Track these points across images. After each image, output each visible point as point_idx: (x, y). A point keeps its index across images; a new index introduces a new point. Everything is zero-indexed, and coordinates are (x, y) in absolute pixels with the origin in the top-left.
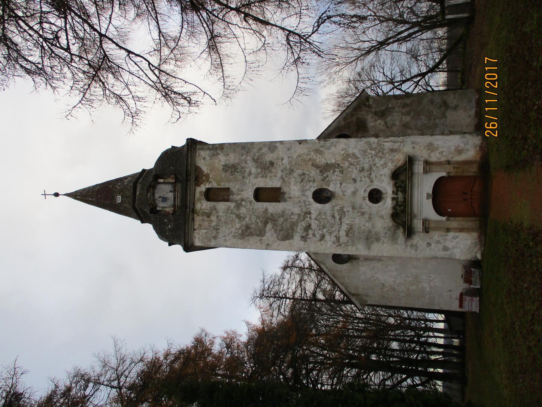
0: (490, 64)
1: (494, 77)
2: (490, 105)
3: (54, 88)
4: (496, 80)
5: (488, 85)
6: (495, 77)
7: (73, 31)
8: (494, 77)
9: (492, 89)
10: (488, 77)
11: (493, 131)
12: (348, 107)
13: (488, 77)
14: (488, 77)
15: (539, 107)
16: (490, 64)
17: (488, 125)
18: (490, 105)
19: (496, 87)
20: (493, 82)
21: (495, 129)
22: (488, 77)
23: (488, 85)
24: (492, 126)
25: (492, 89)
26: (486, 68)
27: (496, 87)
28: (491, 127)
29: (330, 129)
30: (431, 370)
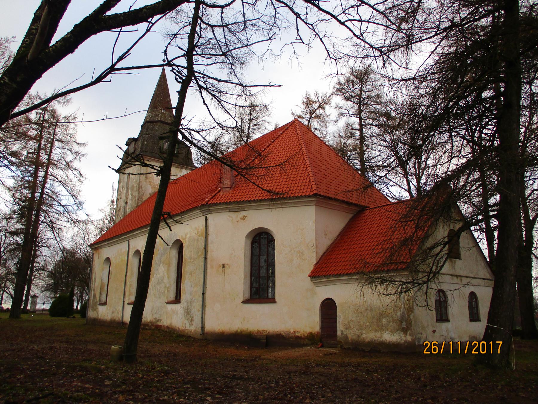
0: (496, 346)
1: (483, 351)
8: (483, 351)
10: (483, 344)
13: (483, 344)
14: (483, 344)
16: (496, 346)
20: (478, 350)
21: (431, 352)
22: (483, 344)
26: (491, 343)
28: (433, 347)
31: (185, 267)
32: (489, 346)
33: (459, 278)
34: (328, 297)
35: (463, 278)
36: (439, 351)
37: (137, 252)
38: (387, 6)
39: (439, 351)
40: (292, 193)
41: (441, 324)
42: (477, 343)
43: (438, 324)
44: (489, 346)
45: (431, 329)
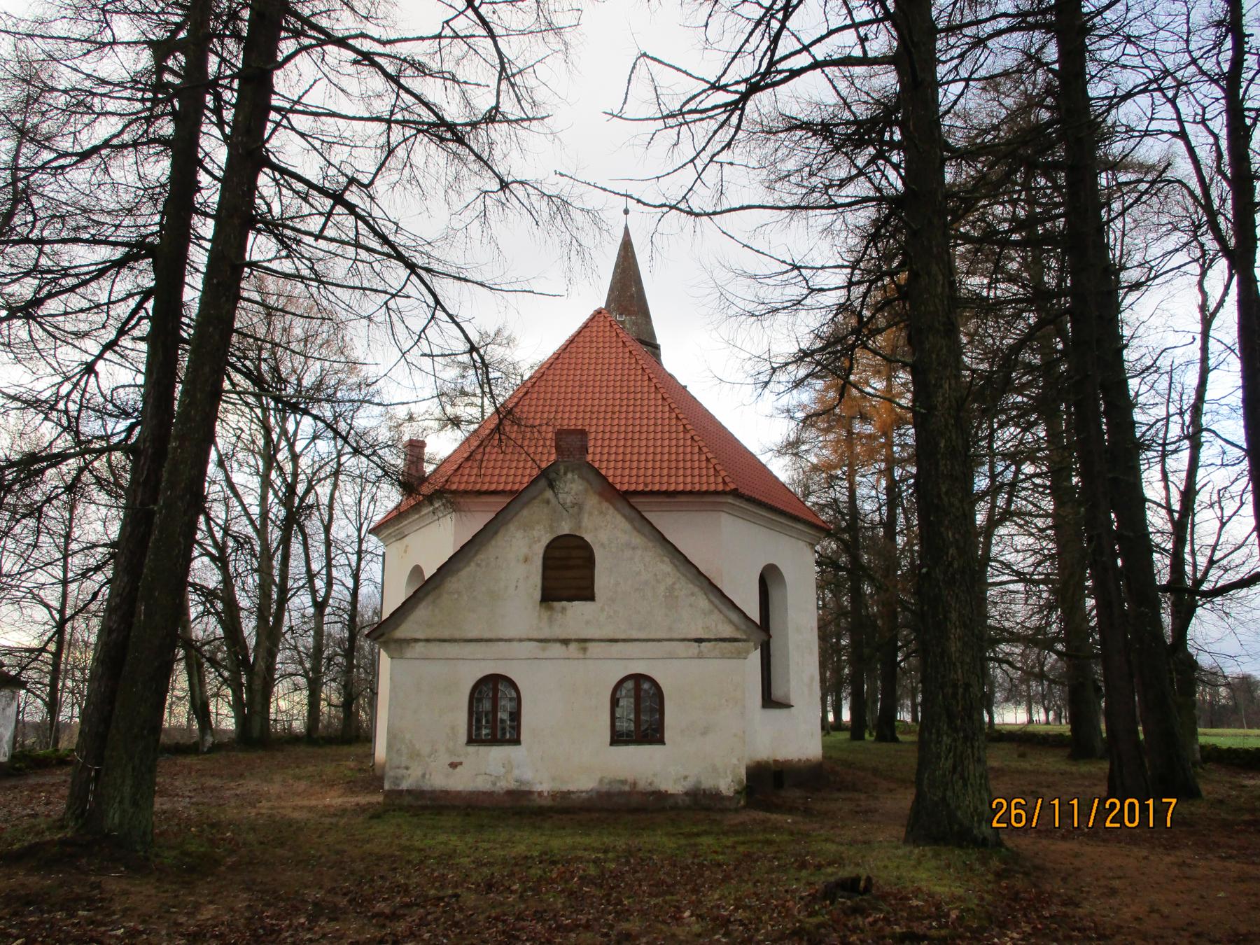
0: (1161, 811)
1: (1132, 820)
2: (1066, 813)
3: (678, 117)
4: (1122, 823)
5: (1113, 805)
6: (1132, 821)
7: (806, 123)
8: (1132, 820)
9: (1102, 814)
10: (1132, 805)
11: (1006, 818)
12: (535, 498)
13: (1132, 804)
14: (1132, 805)
15: (272, 931)
16: (1161, 811)
17: (1018, 806)
18: (1066, 813)
19: (1108, 824)
20: (1119, 818)
21: (1009, 822)
22: (1132, 804)
23: (1113, 805)
24: (1017, 815)
25: (1102, 814)
26: (1151, 802)
27: (1108, 824)
28: (1014, 812)
29: (443, 470)
30: (1140, 728)
31: (711, 602)
32: (1144, 809)
33: (573, 646)
34: (480, 675)
35: (590, 645)
36: (1029, 820)
37: (417, 570)
38: (44, 261)
39: (1029, 820)
40: (498, 483)
41: (483, 750)
42: (1117, 801)
43: (472, 749)
44: (1144, 809)
45: (446, 759)
